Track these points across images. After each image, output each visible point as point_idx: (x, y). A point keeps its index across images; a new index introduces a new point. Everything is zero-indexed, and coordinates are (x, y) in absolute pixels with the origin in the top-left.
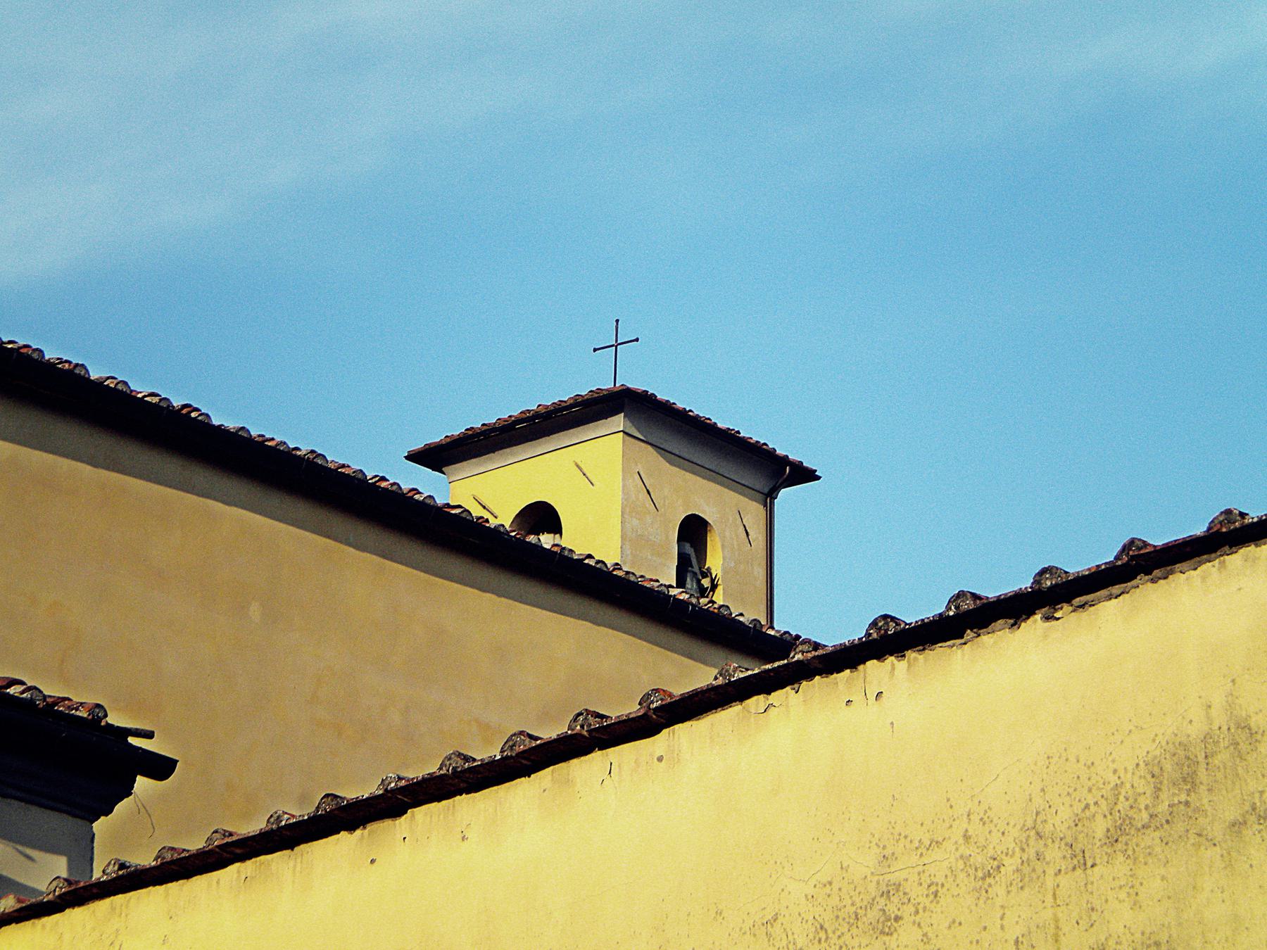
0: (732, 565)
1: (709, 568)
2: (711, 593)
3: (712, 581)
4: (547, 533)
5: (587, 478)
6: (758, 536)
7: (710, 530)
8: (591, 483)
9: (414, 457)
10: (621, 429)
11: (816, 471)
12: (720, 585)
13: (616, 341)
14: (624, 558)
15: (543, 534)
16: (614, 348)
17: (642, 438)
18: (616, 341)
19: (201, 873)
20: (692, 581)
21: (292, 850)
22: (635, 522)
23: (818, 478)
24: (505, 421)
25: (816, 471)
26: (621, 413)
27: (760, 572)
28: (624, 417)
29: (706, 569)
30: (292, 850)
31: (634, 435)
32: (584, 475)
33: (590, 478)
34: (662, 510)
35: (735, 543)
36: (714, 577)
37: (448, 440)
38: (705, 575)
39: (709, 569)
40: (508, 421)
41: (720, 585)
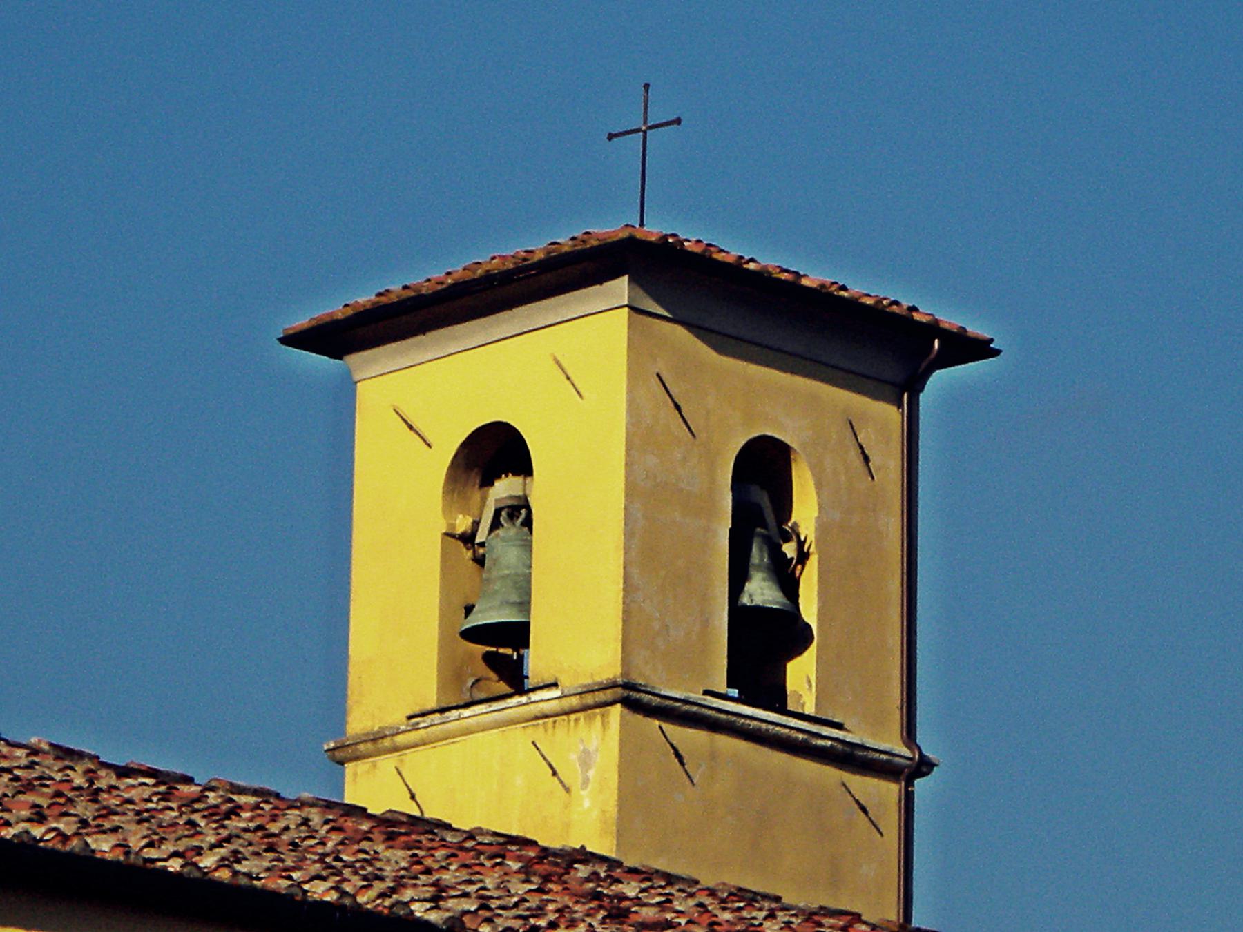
0: (837, 516)
1: (795, 524)
2: (799, 567)
3: (801, 544)
4: (513, 475)
5: (573, 385)
6: (889, 463)
7: (795, 460)
8: (578, 393)
9: (296, 339)
10: (626, 303)
11: (992, 340)
12: (813, 553)
13: (645, 122)
14: (630, 527)
15: (507, 476)
16: (641, 133)
17: (666, 314)
18: (645, 122)
19: (526, 303)
20: (761, 550)
21: (583, 847)
22: (651, 460)
23: (996, 353)
24: (438, 283)
25: (992, 340)
26: (623, 275)
27: (893, 526)
28: (630, 281)
29: (791, 528)
30: (583, 847)
31: (650, 310)
32: (568, 378)
33: (579, 387)
34: (702, 436)
35: (843, 478)
36: (802, 538)
37: (350, 312)
38: (787, 539)
39: (795, 528)
40: (442, 283)
41: (813, 553)
